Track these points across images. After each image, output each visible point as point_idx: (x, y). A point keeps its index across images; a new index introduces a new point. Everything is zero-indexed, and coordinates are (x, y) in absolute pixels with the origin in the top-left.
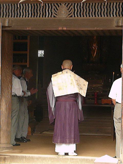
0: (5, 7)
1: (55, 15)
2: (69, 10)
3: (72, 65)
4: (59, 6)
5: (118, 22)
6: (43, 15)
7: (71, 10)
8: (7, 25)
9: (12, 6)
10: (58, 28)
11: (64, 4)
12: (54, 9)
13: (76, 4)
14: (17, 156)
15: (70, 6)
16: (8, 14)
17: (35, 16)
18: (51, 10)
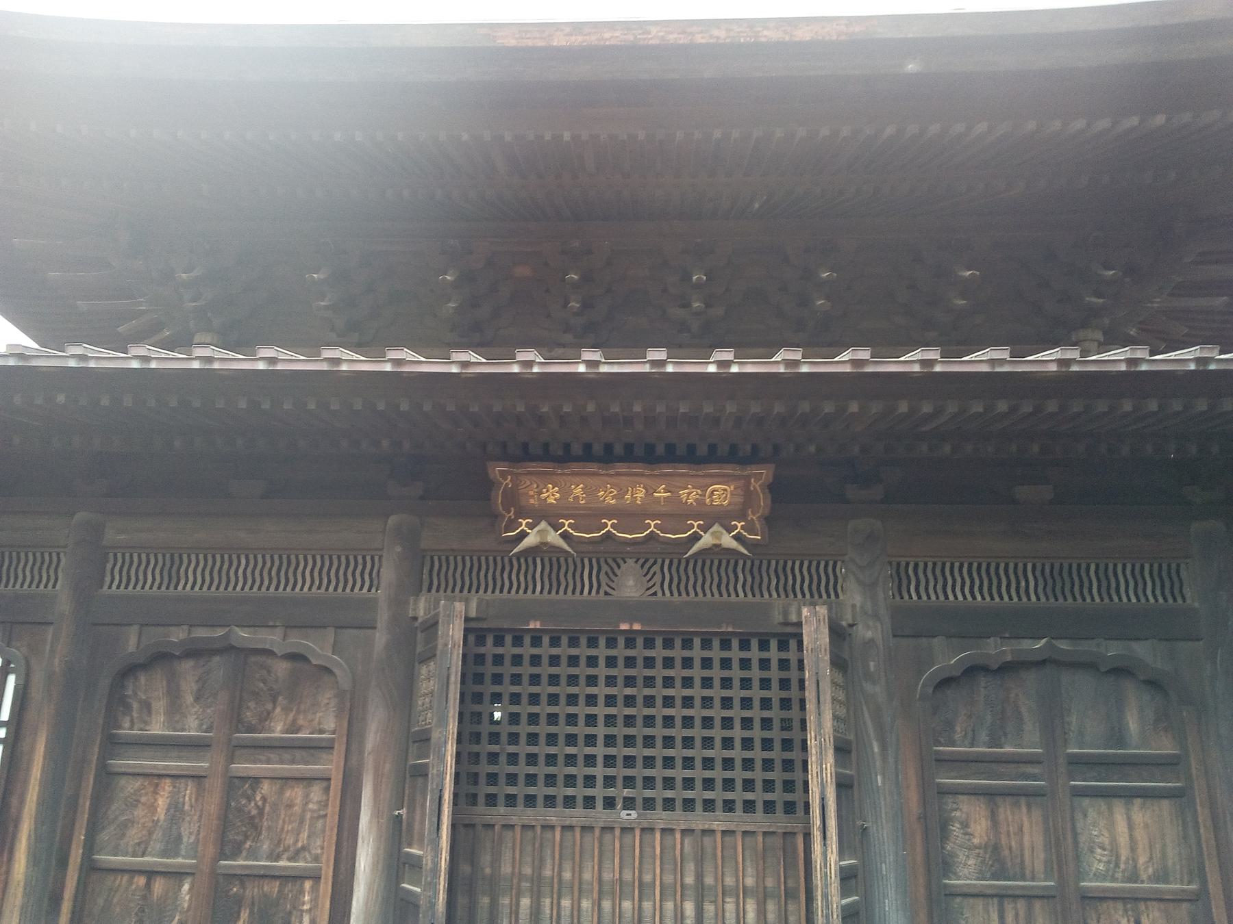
0: (277, 563)
1: (608, 590)
3: (130, 786)
5: (786, 613)
6: (526, 589)
8: (473, 614)
9: (11, 558)
12: (606, 573)
13: (667, 562)
16: (523, 585)
17: (554, 592)
18: (598, 576)
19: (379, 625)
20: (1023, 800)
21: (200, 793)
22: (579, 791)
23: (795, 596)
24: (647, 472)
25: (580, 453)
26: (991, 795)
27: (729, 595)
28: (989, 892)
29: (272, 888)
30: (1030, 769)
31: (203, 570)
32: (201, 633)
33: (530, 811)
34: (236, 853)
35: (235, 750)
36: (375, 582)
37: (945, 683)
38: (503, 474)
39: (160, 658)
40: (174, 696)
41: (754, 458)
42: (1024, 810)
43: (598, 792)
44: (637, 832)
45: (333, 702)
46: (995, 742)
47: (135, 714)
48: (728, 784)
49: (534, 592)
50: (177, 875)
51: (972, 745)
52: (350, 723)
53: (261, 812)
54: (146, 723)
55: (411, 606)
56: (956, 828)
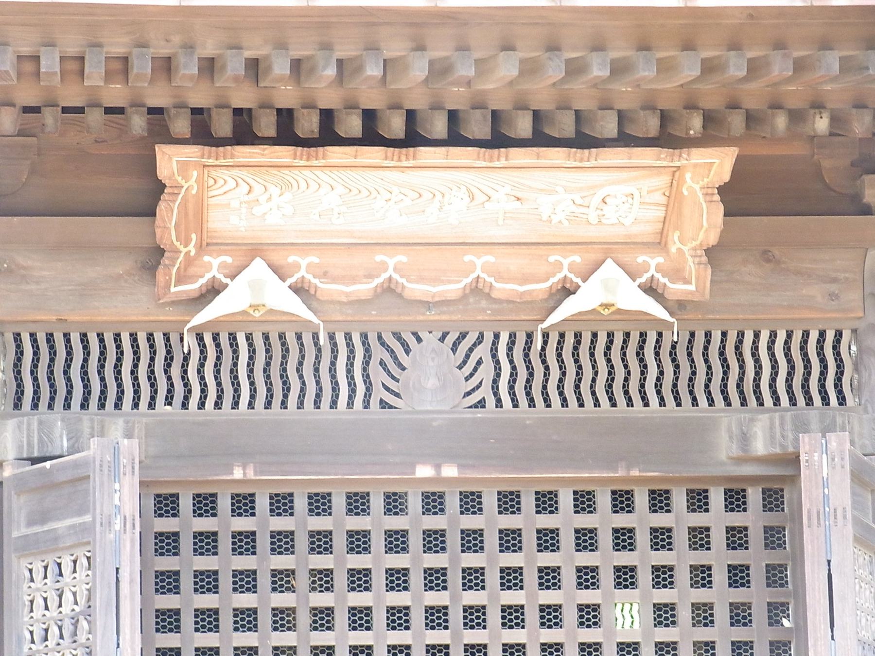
4: (407, 351)
5: (745, 439)
7: (475, 369)
10: (413, 467)
11: (440, 335)
12: (382, 363)
15: (471, 350)
25: (272, 132)
38: (184, 167)
41: (713, 132)
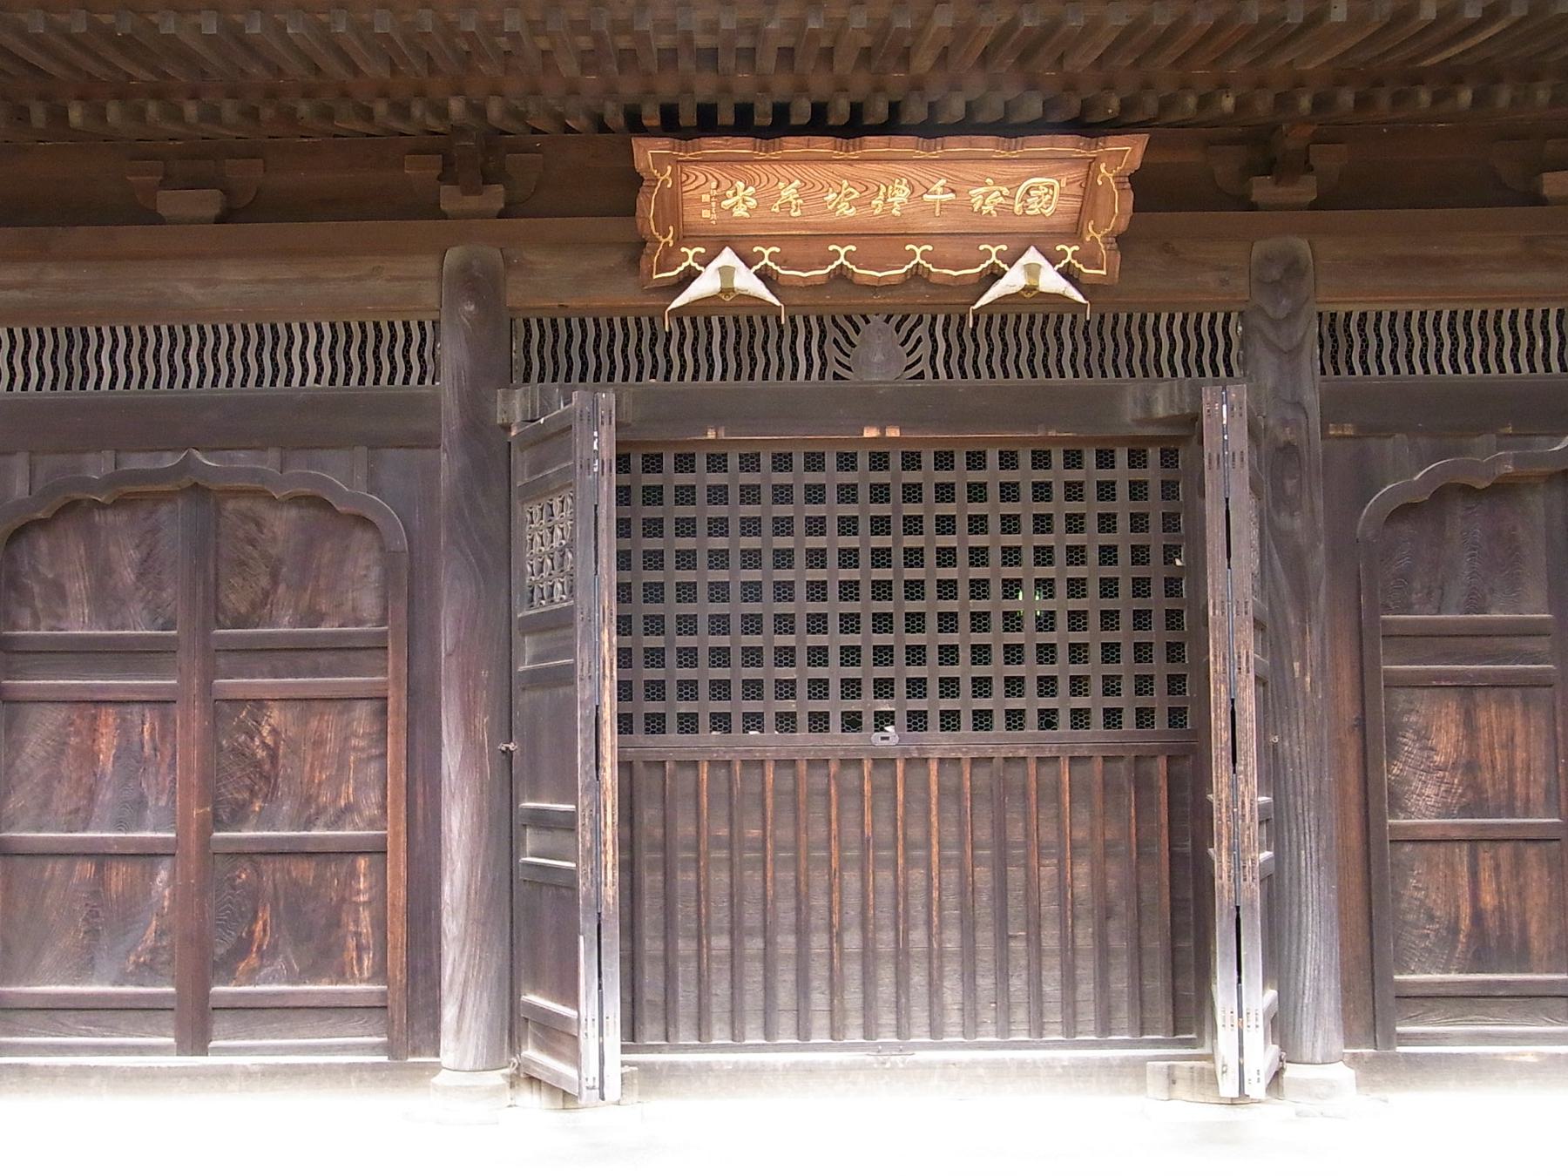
2: (909, 346)
5: (1148, 403)
6: (781, 370)
7: (915, 347)
12: (836, 342)
14: (673, 1067)
15: (911, 330)
19: (445, 440)
20: (1516, 694)
21: (165, 731)
22: (771, 706)
23: (1160, 374)
24: (923, 154)
26: (1466, 688)
27: (1048, 375)
28: (1455, 834)
29: (305, 871)
30: (1529, 645)
31: (127, 356)
32: (138, 462)
33: (853, 737)
34: (238, 816)
35: (218, 657)
36: (430, 367)
37: (1404, 512)
39: (72, 509)
40: (102, 574)
41: (1117, 126)
42: (1518, 708)
43: (835, 705)
44: (900, 765)
45: (375, 573)
46: (1475, 603)
47: (39, 604)
48: (949, 687)
49: (710, 377)
50: (148, 855)
51: (1439, 613)
52: (410, 603)
53: (273, 756)
54: (59, 618)
55: (500, 406)
56: (1408, 741)
